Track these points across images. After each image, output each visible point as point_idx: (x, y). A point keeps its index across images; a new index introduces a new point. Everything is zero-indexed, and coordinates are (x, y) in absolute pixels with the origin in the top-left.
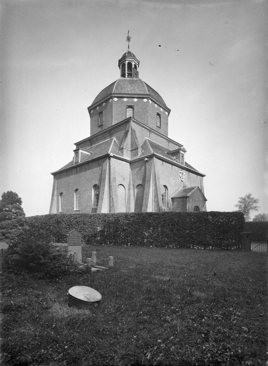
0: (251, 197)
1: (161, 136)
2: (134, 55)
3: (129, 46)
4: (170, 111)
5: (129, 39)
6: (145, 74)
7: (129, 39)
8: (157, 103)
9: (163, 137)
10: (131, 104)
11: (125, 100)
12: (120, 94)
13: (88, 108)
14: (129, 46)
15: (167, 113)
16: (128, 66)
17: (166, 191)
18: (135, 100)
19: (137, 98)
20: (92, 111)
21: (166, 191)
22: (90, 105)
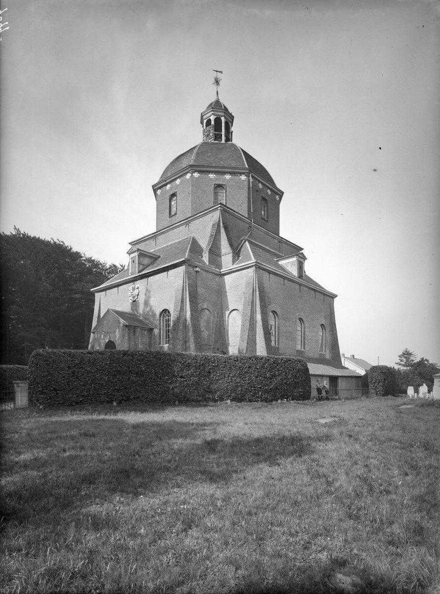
0: (408, 350)
1: (174, 227)
2: (225, 107)
3: (217, 92)
4: (283, 194)
5: (217, 82)
6: (241, 138)
7: (217, 82)
8: (167, 181)
9: (176, 227)
10: (221, 183)
11: (211, 176)
12: (203, 166)
13: (153, 187)
14: (217, 92)
15: (277, 197)
16: (220, 123)
17: (301, 324)
18: (228, 177)
19: (230, 173)
20: (159, 192)
21: (301, 324)
22: (156, 181)
